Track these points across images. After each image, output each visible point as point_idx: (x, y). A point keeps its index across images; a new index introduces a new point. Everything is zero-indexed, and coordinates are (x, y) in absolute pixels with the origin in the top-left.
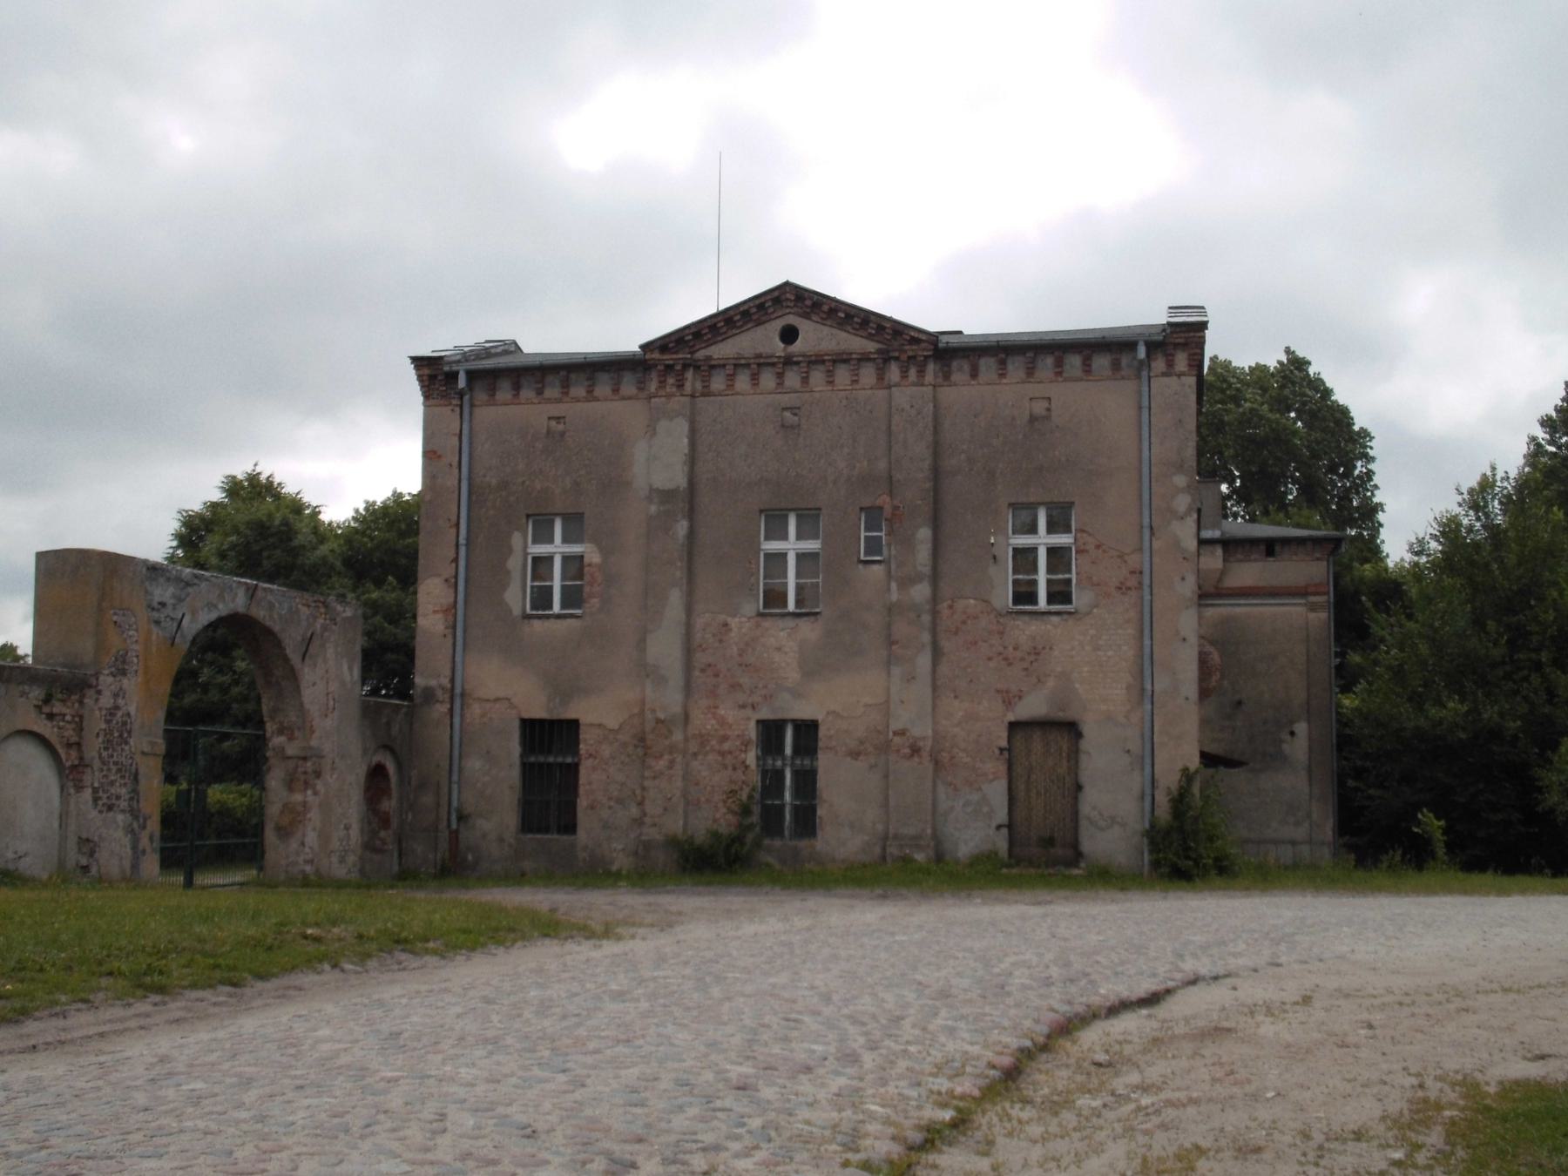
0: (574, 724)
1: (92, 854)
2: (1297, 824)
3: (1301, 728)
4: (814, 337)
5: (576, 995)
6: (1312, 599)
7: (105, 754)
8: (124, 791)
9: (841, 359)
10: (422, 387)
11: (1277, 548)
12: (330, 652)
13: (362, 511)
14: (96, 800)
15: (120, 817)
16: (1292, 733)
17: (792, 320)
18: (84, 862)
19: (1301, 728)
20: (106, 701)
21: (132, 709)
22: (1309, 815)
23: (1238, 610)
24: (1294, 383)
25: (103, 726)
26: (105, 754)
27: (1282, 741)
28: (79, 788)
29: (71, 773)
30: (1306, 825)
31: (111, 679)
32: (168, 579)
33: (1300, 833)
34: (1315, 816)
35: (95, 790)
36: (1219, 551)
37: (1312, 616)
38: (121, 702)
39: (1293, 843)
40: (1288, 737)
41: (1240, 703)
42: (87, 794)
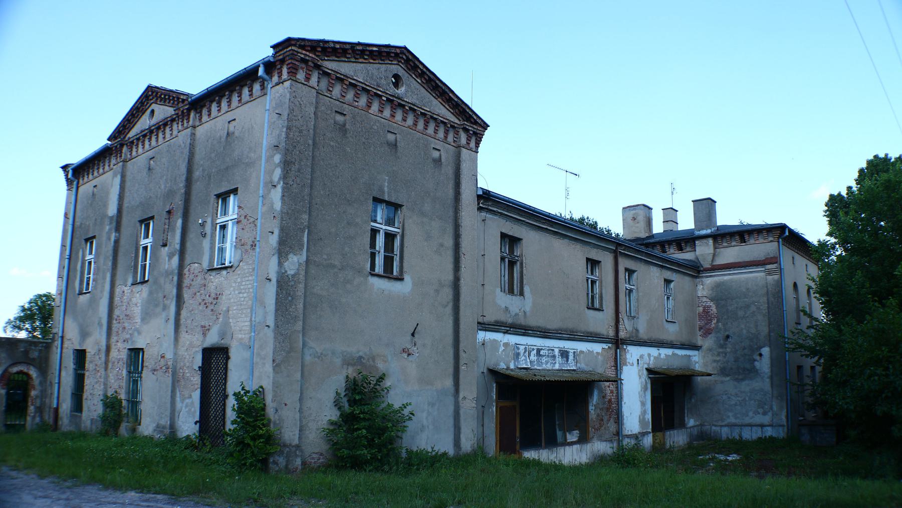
2: (765, 414)
3: (766, 351)
4: (411, 91)
5: (253, 452)
6: (769, 267)
9: (439, 122)
10: (171, 91)
11: (746, 237)
16: (761, 355)
17: (401, 72)
19: (766, 351)
22: (771, 408)
23: (726, 278)
24: (869, 163)
27: (755, 360)
30: (770, 414)
33: (766, 419)
34: (775, 408)
36: (711, 241)
37: (770, 278)
39: (762, 426)
40: (758, 358)
41: (728, 337)
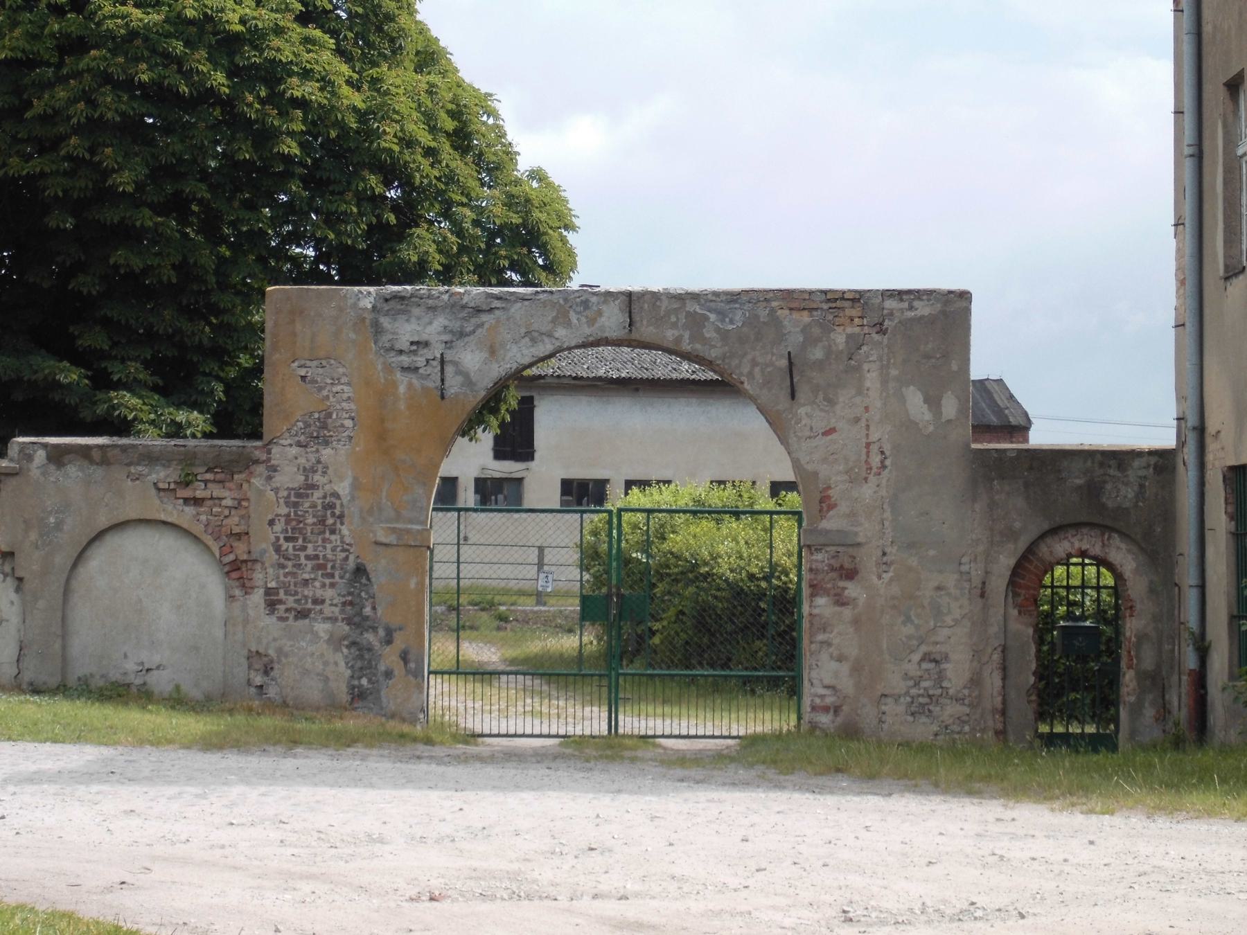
0: (477, 480)
1: (267, 671)
7: (288, 547)
8: (329, 593)
12: (872, 379)
13: (563, 194)
14: (272, 605)
15: (322, 628)
18: (258, 680)
20: (289, 477)
21: (343, 488)
25: (284, 510)
26: (288, 547)
28: (247, 589)
29: (237, 571)
31: (294, 451)
32: (432, 309)
35: (268, 591)
38: (317, 478)
42: (258, 597)
